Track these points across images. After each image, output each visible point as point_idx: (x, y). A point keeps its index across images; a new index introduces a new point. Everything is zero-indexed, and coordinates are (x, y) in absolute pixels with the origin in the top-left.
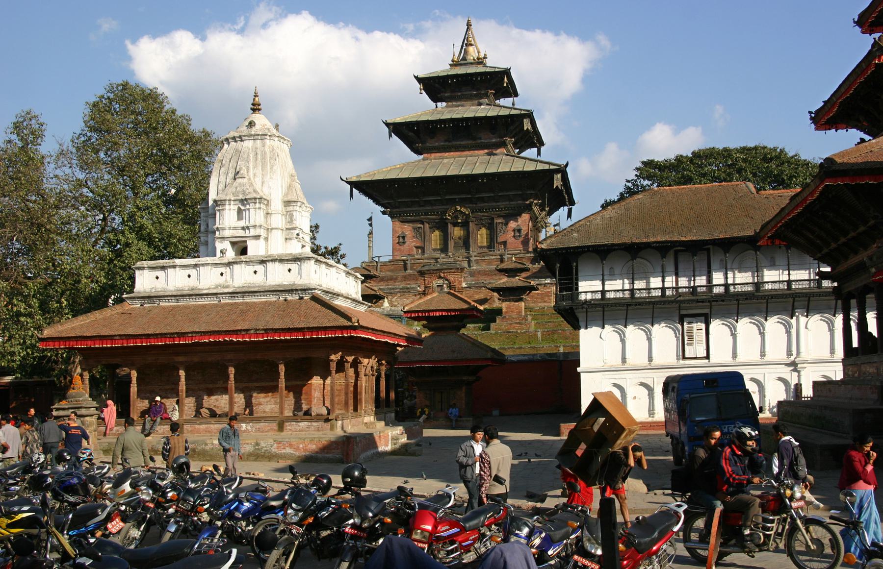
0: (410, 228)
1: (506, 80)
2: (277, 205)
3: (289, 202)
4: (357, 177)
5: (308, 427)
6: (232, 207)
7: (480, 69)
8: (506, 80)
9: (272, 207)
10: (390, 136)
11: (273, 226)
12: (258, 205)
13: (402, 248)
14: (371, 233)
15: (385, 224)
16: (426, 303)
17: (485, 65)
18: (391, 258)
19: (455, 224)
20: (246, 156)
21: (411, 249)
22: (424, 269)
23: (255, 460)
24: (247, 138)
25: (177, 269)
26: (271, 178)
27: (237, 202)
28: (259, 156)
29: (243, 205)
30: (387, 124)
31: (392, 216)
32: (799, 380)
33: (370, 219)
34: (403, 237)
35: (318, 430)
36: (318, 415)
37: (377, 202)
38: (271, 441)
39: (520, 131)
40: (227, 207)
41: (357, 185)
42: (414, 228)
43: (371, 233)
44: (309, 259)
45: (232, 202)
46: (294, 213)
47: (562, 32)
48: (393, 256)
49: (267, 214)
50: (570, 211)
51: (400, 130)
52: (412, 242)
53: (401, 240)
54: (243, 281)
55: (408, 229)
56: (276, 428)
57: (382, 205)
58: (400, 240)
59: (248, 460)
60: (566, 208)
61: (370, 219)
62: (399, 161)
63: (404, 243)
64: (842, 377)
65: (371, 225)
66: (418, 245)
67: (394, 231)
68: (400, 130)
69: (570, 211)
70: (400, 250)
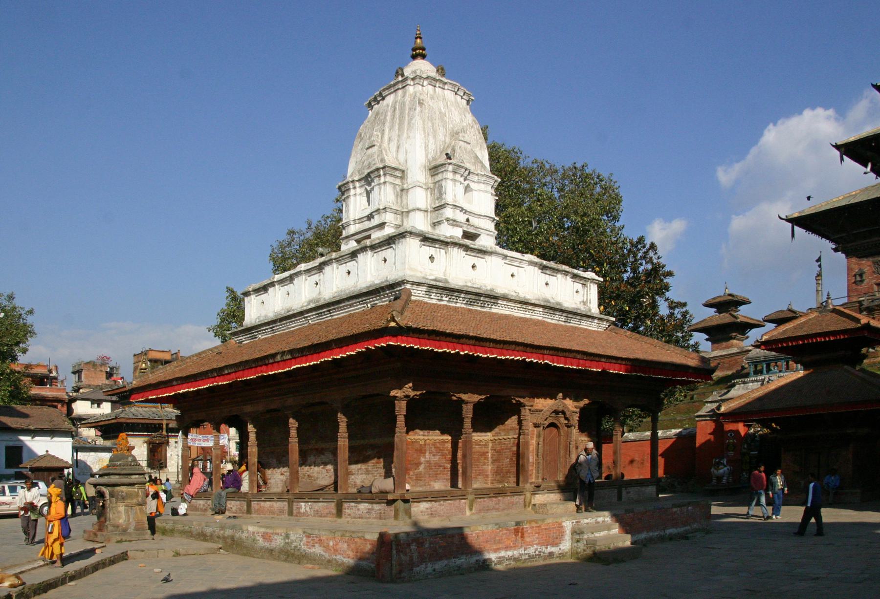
0: (869, 263)
2: (417, 174)
3: (436, 167)
4: (800, 212)
5: (369, 511)
6: (358, 191)
9: (409, 180)
10: (842, 159)
11: (410, 208)
12: (382, 179)
13: (859, 287)
14: (819, 275)
15: (837, 263)
16: (795, 328)
18: (845, 300)
20: (382, 118)
21: (871, 287)
22: (872, 304)
23: (285, 560)
24: (387, 92)
25: (277, 287)
26: (408, 137)
27: (363, 183)
28: (397, 112)
29: (369, 184)
30: (837, 147)
31: (848, 254)
33: (819, 260)
34: (861, 275)
35: (380, 518)
36: (381, 492)
37: (823, 235)
38: (300, 532)
40: (352, 192)
41: (797, 221)
42: (874, 263)
43: (819, 275)
44: (491, 253)
45: (357, 184)
46: (444, 183)
48: (849, 296)
49: (402, 190)
53: (858, 278)
54: (335, 290)
55: (866, 265)
56: (334, 511)
57: (832, 240)
58: (857, 279)
59: (278, 559)
61: (819, 260)
63: (862, 281)
65: (820, 266)
67: (849, 269)
70: (856, 290)
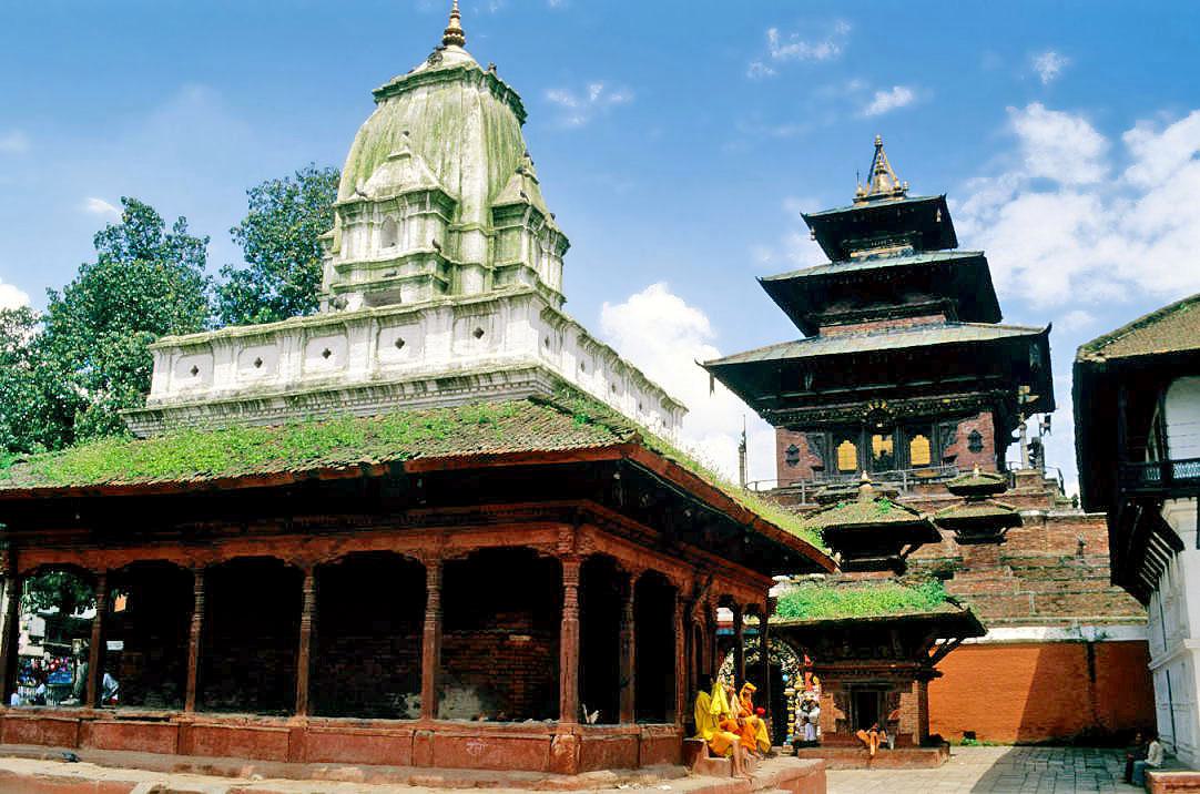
1: (939, 213)
7: (900, 200)
8: (939, 213)
15: (765, 438)
17: (905, 197)
18: (776, 486)
19: (878, 431)
32: (452, 345)
39: (967, 288)
47: (1009, 108)
50: (1048, 419)
51: (781, 291)
52: (808, 460)
58: (789, 457)
60: (1042, 416)
62: (777, 336)
64: (1164, 514)
66: (817, 464)
67: (780, 444)
68: (781, 291)
69: (1048, 419)
